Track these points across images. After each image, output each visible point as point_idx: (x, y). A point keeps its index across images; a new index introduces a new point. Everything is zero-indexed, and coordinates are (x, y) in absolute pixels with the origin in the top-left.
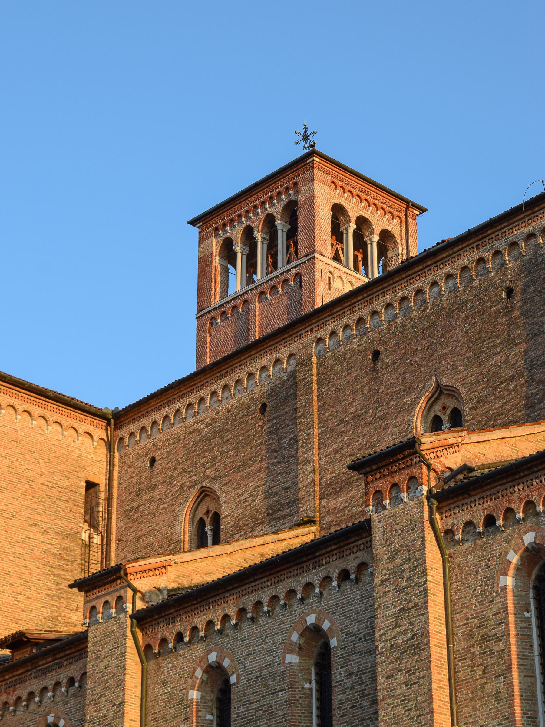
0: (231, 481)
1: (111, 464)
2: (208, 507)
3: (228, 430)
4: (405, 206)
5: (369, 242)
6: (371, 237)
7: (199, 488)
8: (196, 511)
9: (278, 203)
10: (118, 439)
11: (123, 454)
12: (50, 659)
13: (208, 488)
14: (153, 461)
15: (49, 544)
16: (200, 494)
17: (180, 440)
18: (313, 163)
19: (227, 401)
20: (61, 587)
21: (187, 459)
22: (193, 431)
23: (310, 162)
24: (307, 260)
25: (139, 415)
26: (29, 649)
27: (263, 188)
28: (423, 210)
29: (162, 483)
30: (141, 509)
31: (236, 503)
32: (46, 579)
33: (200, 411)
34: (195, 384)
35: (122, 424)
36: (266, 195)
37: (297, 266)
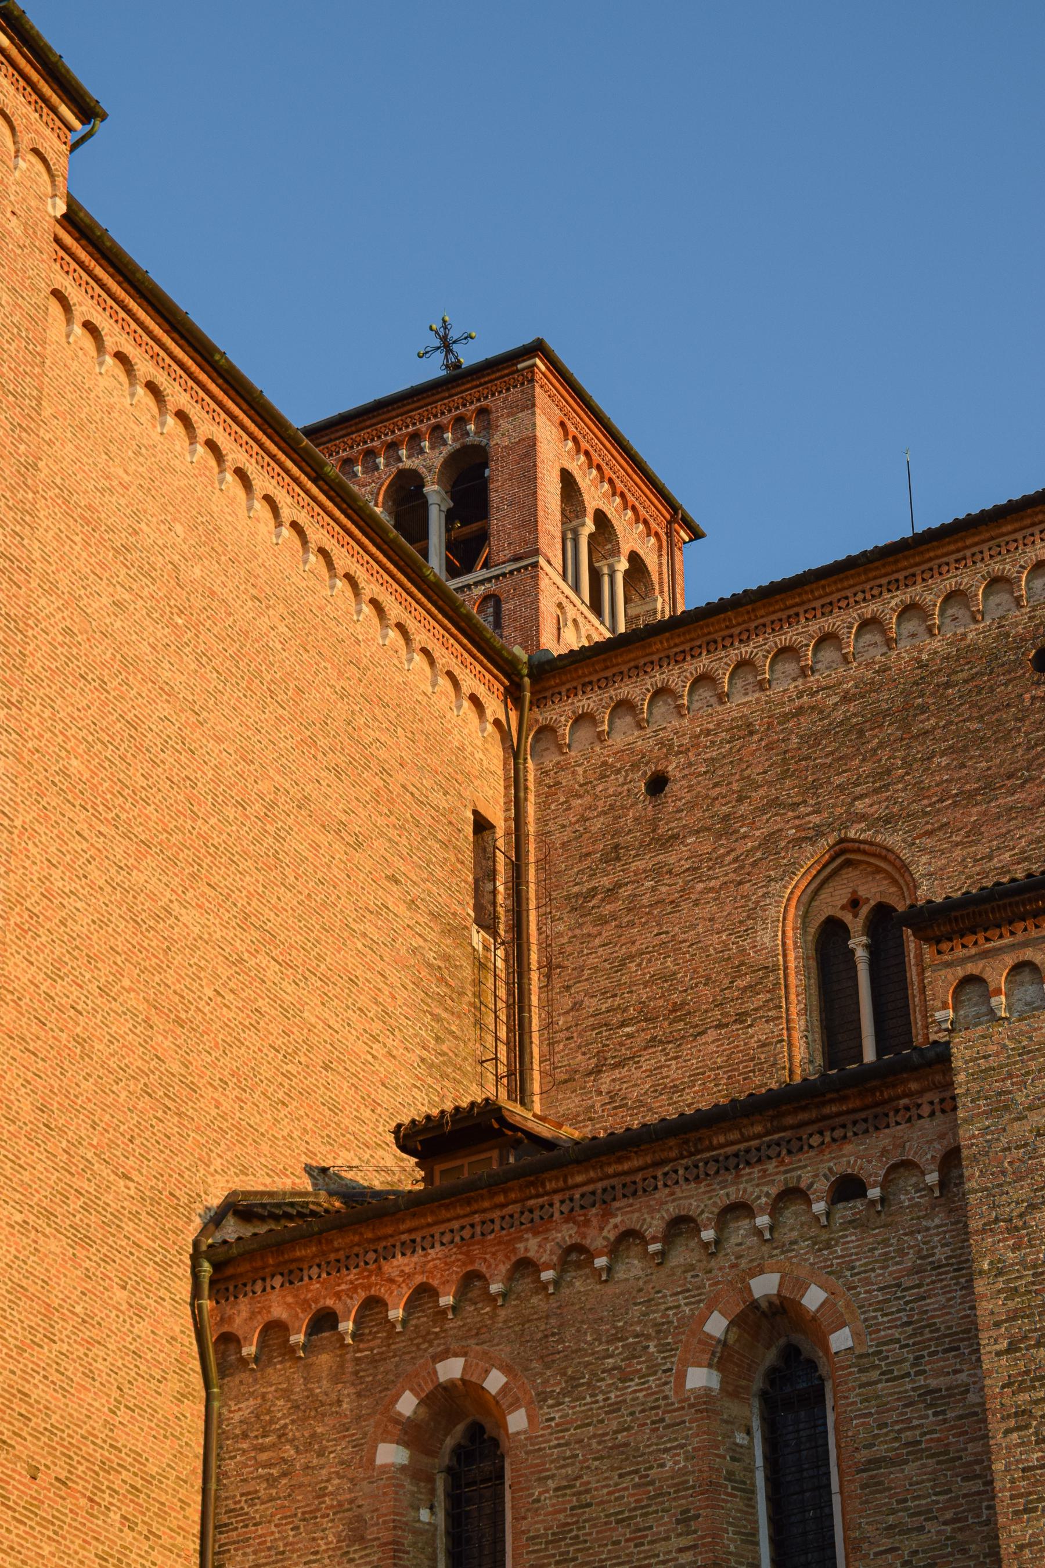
0: (946, 824)
1: (516, 782)
2: (855, 892)
3: (923, 709)
4: (668, 517)
5: (606, 570)
6: (611, 560)
7: (831, 841)
8: (812, 899)
9: (432, 448)
10: (535, 729)
11: (549, 765)
12: (758, 1129)
13: (865, 842)
14: (657, 784)
15: (420, 935)
16: (833, 859)
17: (751, 733)
18: (533, 372)
19: (916, 642)
20: (444, 1048)
21: (785, 775)
22: (800, 711)
23: (523, 369)
24: (518, 570)
25: (608, 673)
26: (495, 1154)
27: (394, 413)
28: (696, 534)
29: (698, 832)
30: (625, 892)
31: (970, 877)
32: (419, 1021)
33: (818, 666)
34: (803, 603)
35: (548, 694)
36: (400, 429)
37: (489, 580)
